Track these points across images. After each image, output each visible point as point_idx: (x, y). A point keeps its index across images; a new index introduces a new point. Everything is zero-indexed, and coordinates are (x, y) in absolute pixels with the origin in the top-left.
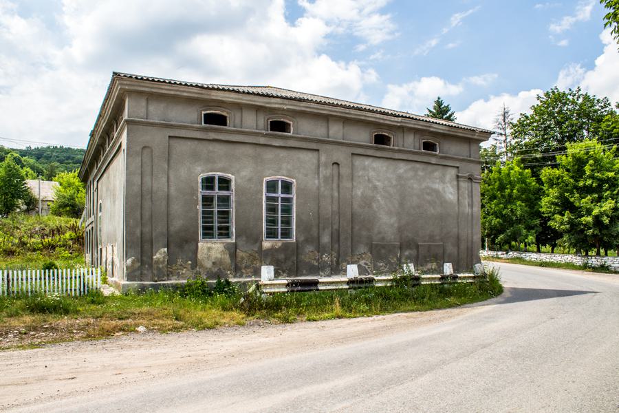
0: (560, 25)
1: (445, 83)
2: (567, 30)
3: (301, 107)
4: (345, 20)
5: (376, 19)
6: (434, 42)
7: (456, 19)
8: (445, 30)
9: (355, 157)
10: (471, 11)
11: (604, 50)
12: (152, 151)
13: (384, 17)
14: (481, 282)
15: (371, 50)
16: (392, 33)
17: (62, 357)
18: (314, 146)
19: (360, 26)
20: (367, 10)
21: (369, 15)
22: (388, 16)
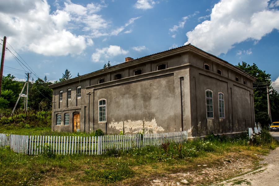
0: (173, 29)
1: (121, 49)
2: (175, 31)
3: (226, 65)
4: (80, 15)
5: (95, 16)
6: (121, 30)
7: (131, 21)
8: (127, 25)
9: (234, 87)
10: (137, 18)
11: (79, 36)
12: (195, 79)
13: (98, 16)
14: (141, 106)
15: (90, 32)
16: (102, 23)
17: (252, 147)
18: (227, 81)
19: (87, 19)
20: (91, 12)
21: (92, 14)
22: (101, 16)
